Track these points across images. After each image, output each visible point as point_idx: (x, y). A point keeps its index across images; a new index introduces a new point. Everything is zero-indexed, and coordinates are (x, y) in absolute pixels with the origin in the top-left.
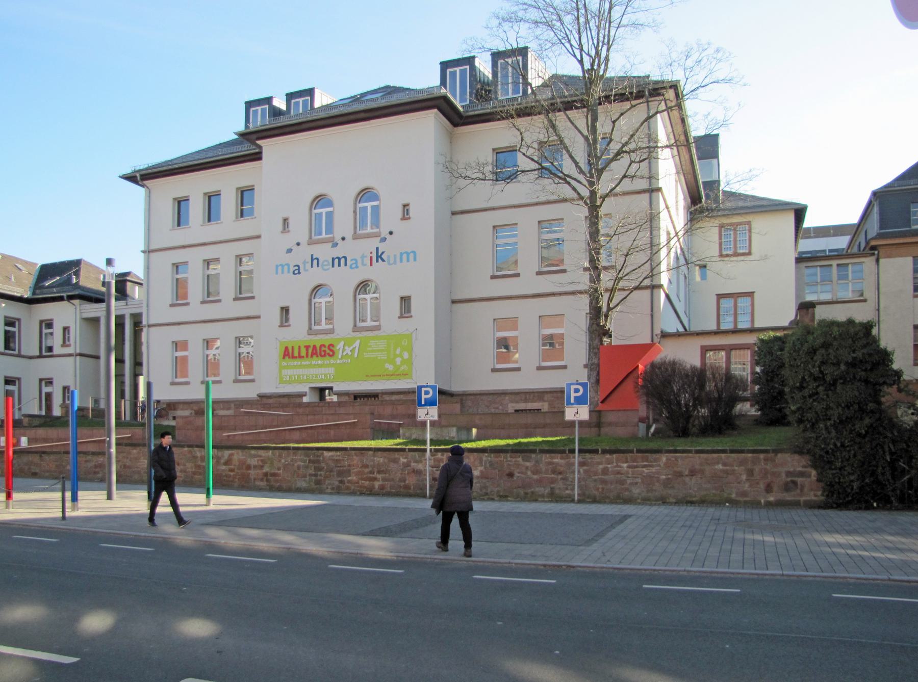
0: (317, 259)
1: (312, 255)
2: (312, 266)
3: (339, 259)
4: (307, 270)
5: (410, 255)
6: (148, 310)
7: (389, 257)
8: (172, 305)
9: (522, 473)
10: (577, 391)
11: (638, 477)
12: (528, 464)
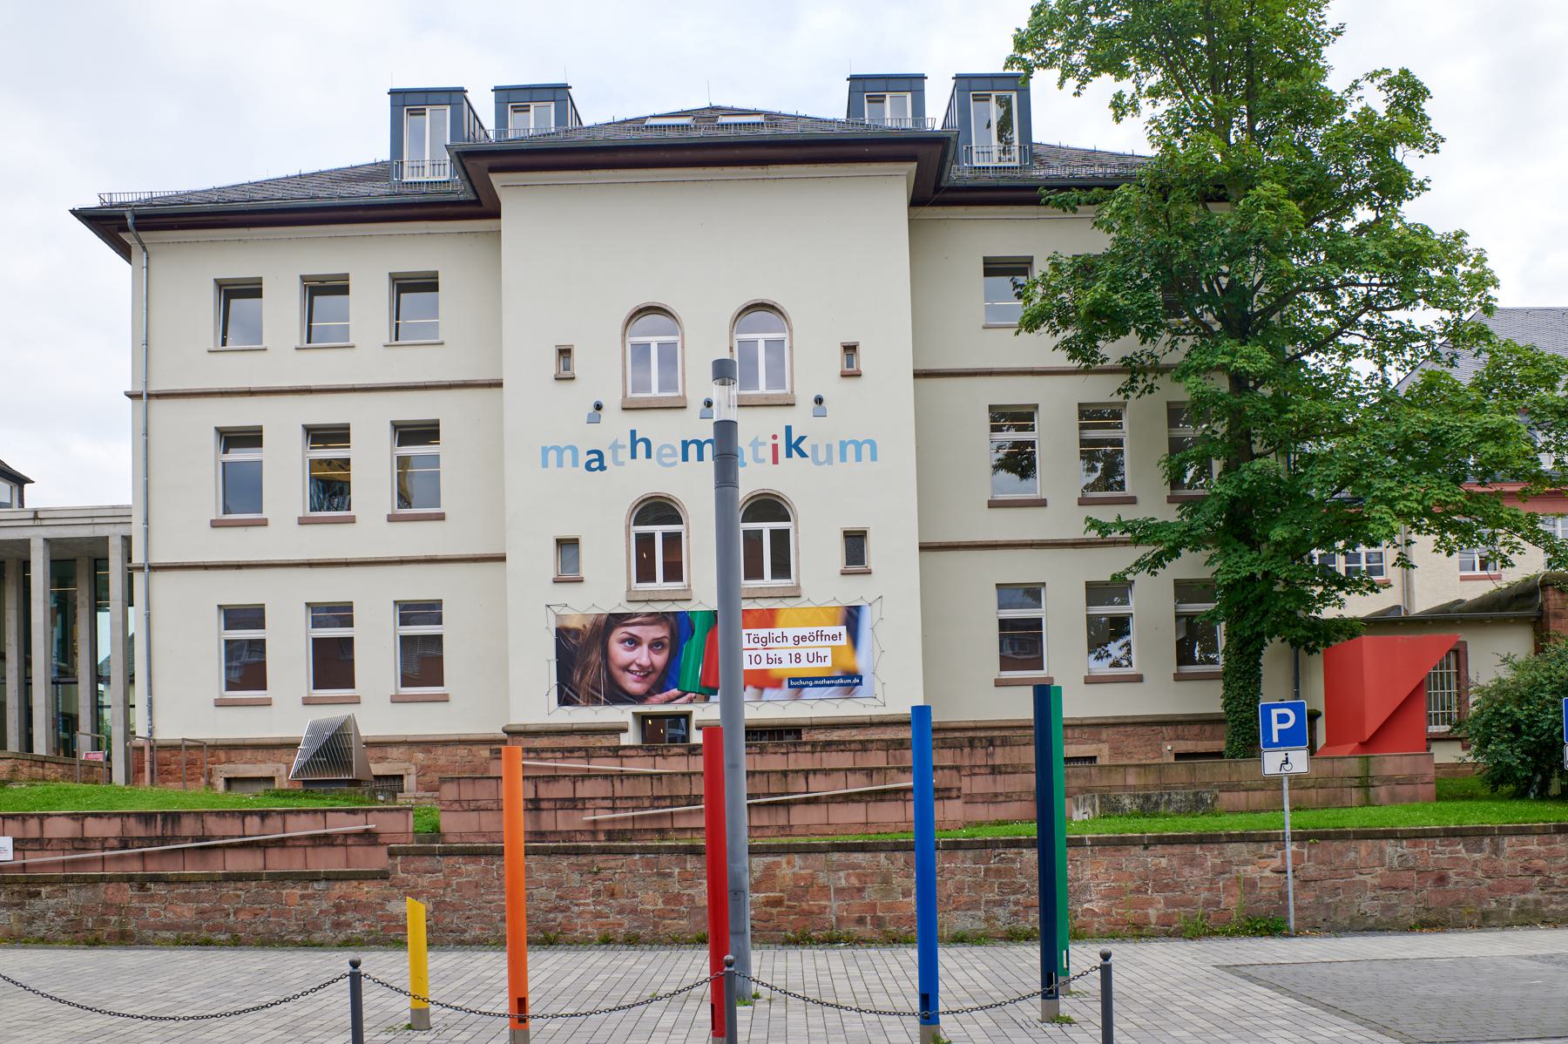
0: (647, 442)
1: (633, 433)
2: (634, 456)
3: (858, 446)
4: (622, 464)
5: (862, 448)
6: (147, 531)
7: (815, 448)
8: (215, 524)
9: (1465, 874)
10: (1283, 719)
11: (1131, 892)
12: (1477, 856)
